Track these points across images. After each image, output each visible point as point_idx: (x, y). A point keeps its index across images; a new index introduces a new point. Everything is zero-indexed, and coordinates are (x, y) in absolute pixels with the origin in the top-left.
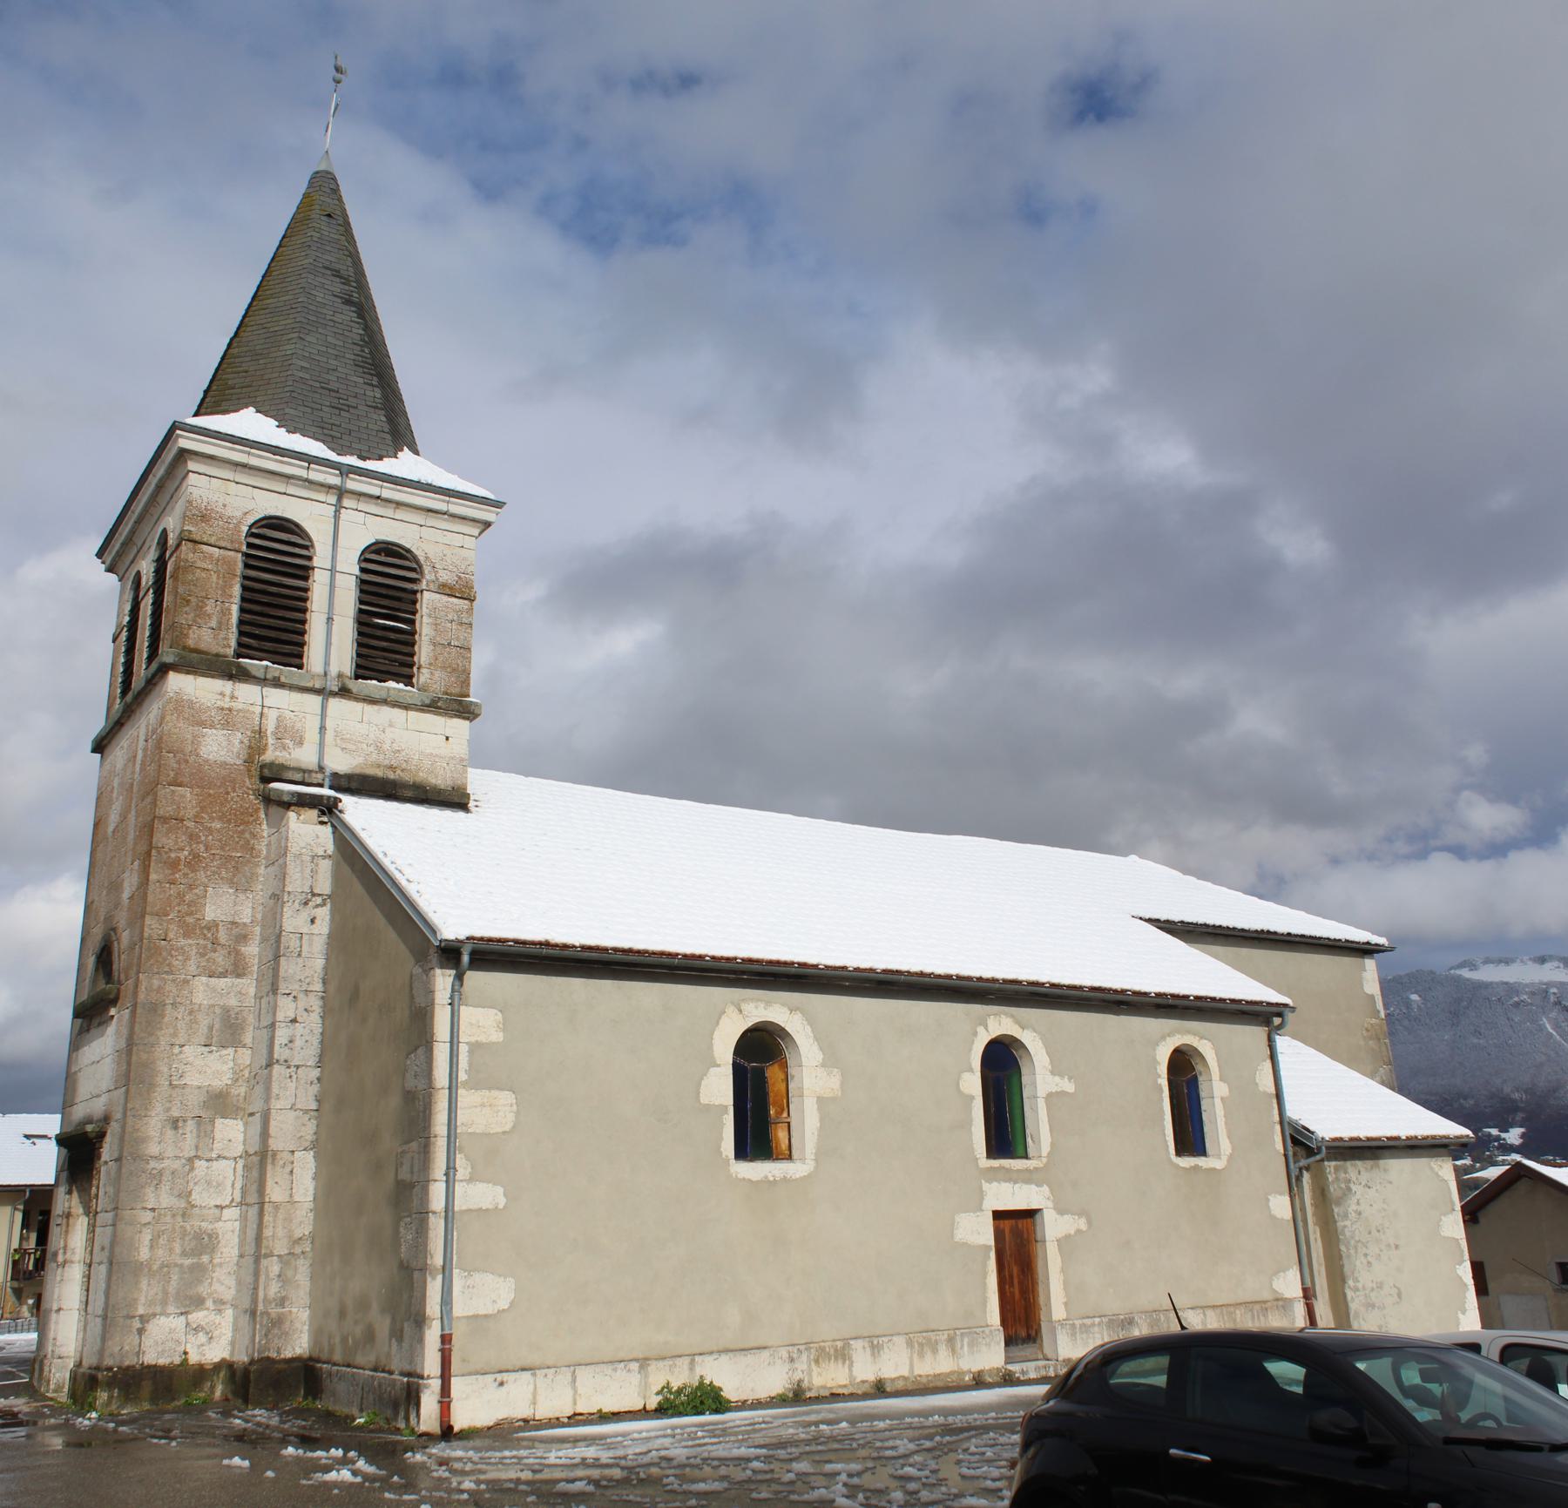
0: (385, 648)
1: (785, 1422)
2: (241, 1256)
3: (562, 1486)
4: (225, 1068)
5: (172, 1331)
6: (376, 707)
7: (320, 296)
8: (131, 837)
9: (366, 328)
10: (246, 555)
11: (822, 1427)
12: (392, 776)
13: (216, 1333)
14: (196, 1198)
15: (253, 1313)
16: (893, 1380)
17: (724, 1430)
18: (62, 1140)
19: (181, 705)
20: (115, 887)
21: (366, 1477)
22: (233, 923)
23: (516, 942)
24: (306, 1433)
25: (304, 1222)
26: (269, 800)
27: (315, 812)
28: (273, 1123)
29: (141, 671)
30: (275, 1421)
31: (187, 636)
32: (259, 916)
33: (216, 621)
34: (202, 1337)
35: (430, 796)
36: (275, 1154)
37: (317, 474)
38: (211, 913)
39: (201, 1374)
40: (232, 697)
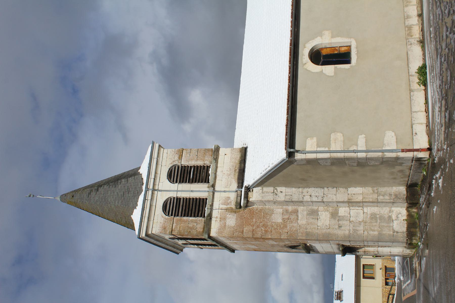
0: (199, 174)
1: (430, 47)
2: (377, 206)
3: (447, 120)
4: (324, 214)
5: (397, 224)
6: (217, 176)
7: (97, 198)
8: (258, 243)
9: (104, 184)
10: (175, 216)
11: (432, 36)
12: (238, 171)
13: (399, 212)
14: (361, 220)
15: (393, 203)
16: (418, 11)
17: (432, 67)
18: (344, 254)
19: (220, 231)
20: (273, 246)
21: (441, 175)
22: (282, 214)
23: (286, 135)
24: (427, 188)
25: (368, 190)
26: (246, 206)
27: (249, 193)
28: (340, 200)
29: (210, 242)
30: (424, 196)
31: (199, 231)
32: (280, 207)
33: (194, 224)
34: (400, 216)
35: (243, 159)
36: (349, 199)
37: (149, 197)
38: (280, 220)
39: (410, 215)
40: (217, 218)
